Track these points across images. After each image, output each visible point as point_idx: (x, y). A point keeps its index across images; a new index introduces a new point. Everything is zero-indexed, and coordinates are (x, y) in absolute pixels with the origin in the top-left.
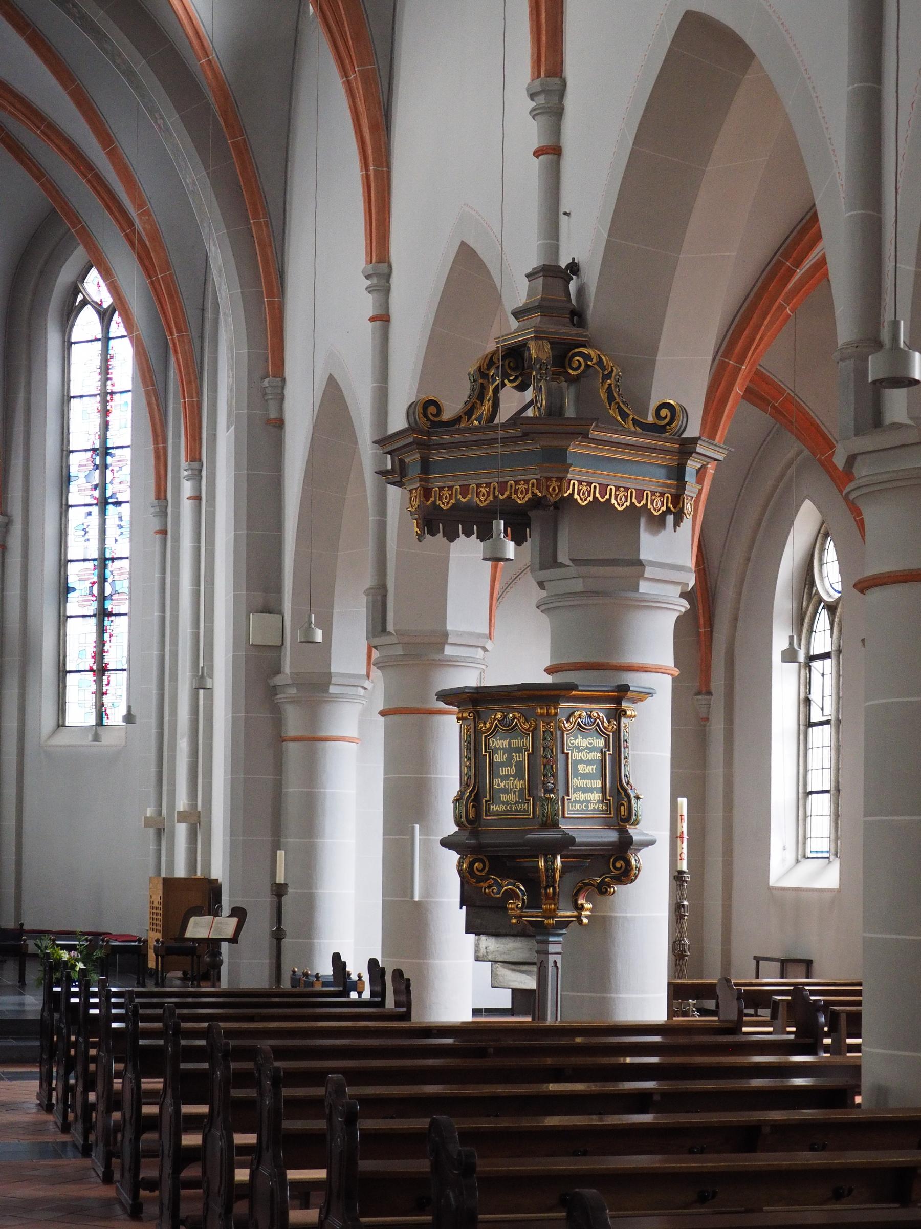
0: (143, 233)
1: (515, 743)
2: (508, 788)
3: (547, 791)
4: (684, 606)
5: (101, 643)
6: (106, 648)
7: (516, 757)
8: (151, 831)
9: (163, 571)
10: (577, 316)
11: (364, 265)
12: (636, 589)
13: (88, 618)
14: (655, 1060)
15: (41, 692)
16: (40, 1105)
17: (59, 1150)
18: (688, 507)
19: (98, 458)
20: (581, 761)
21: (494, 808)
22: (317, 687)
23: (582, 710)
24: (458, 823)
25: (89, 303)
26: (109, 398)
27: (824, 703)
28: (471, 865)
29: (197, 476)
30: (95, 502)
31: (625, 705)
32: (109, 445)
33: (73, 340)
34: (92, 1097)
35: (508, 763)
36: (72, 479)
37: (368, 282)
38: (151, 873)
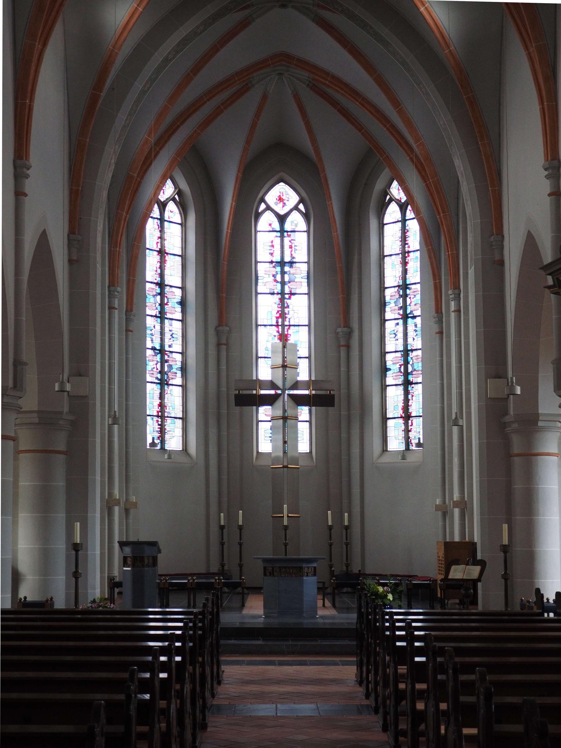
0: (420, 156)
5: (406, 401)
6: (410, 404)
8: (440, 513)
9: (441, 356)
11: (543, 162)
13: (399, 386)
15: (372, 431)
16: (357, 681)
17: (360, 710)
19: (401, 291)
25: (393, 200)
26: (407, 255)
29: (457, 298)
30: (400, 317)
32: (408, 283)
33: (385, 223)
34: (178, 687)
36: (387, 304)
37: (546, 173)
38: (441, 539)
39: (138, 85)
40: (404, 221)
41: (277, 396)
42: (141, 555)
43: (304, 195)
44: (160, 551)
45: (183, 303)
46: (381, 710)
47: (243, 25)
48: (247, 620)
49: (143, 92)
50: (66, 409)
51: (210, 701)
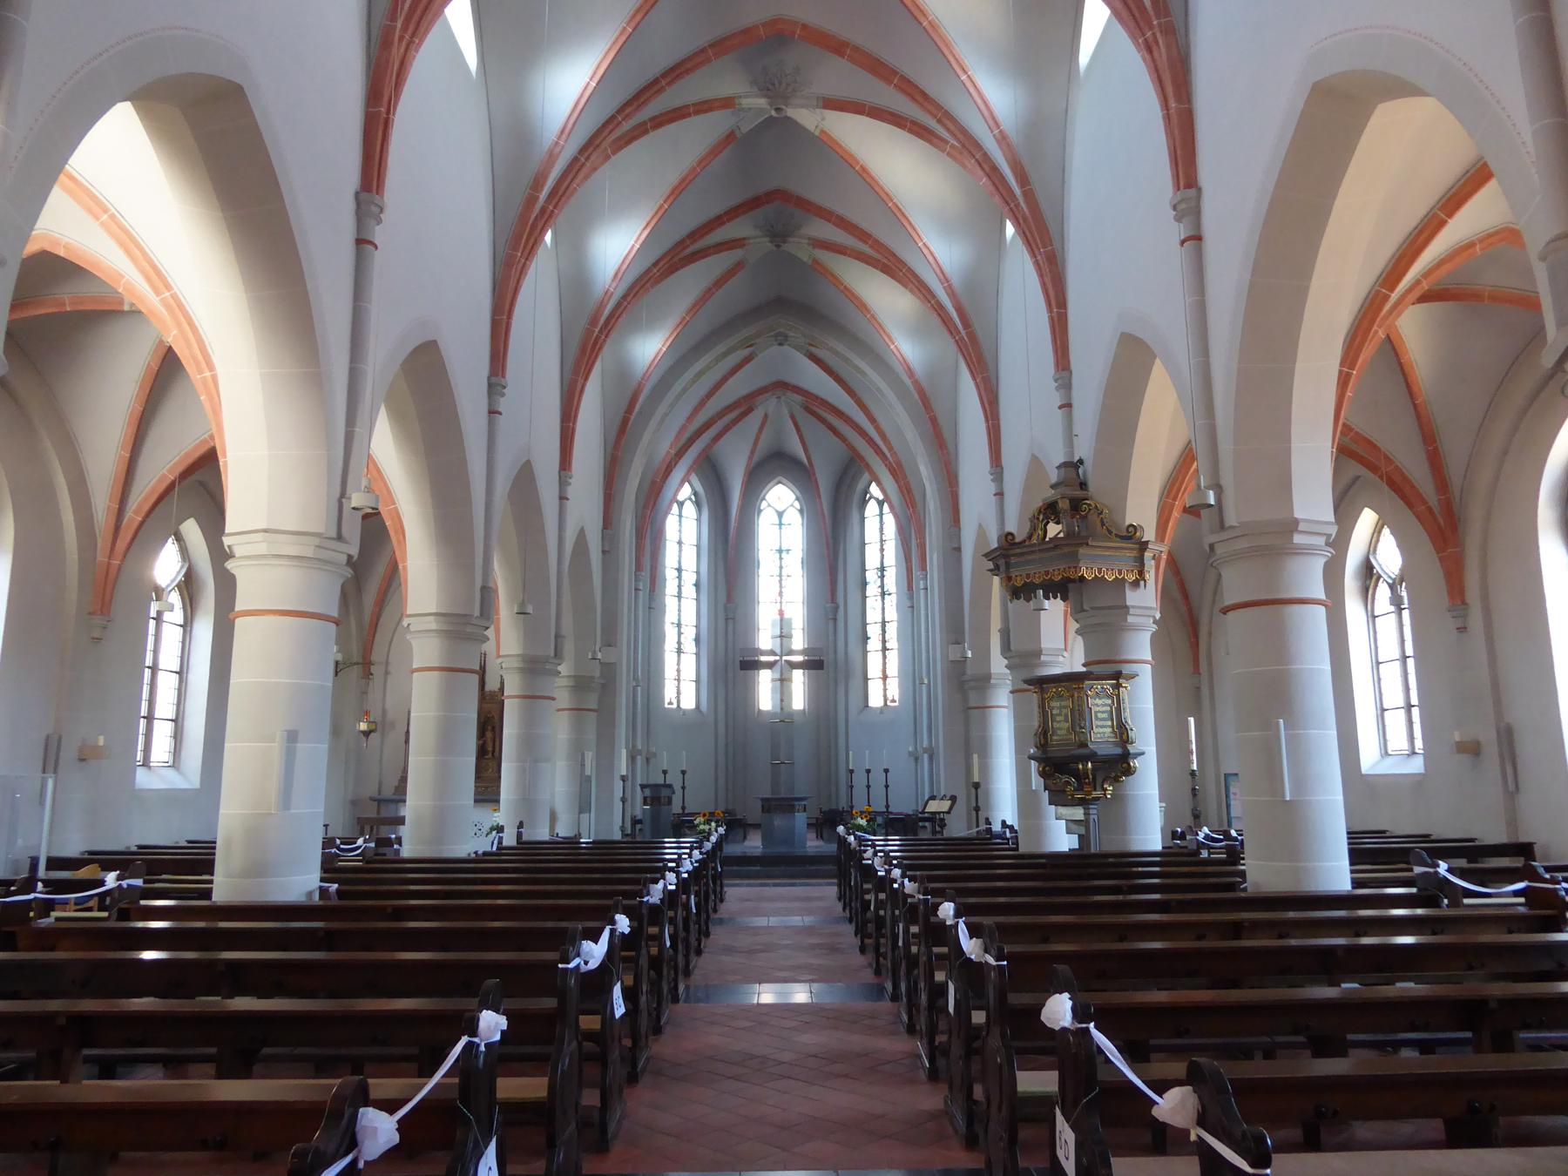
2: (1061, 727)
4: (1154, 628)
10: (1083, 485)
17: (838, 921)
22: (984, 681)
23: (1098, 685)
39: (662, 408)
40: (881, 515)
42: (657, 795)
49: (666, 415)
51: (713, 916)
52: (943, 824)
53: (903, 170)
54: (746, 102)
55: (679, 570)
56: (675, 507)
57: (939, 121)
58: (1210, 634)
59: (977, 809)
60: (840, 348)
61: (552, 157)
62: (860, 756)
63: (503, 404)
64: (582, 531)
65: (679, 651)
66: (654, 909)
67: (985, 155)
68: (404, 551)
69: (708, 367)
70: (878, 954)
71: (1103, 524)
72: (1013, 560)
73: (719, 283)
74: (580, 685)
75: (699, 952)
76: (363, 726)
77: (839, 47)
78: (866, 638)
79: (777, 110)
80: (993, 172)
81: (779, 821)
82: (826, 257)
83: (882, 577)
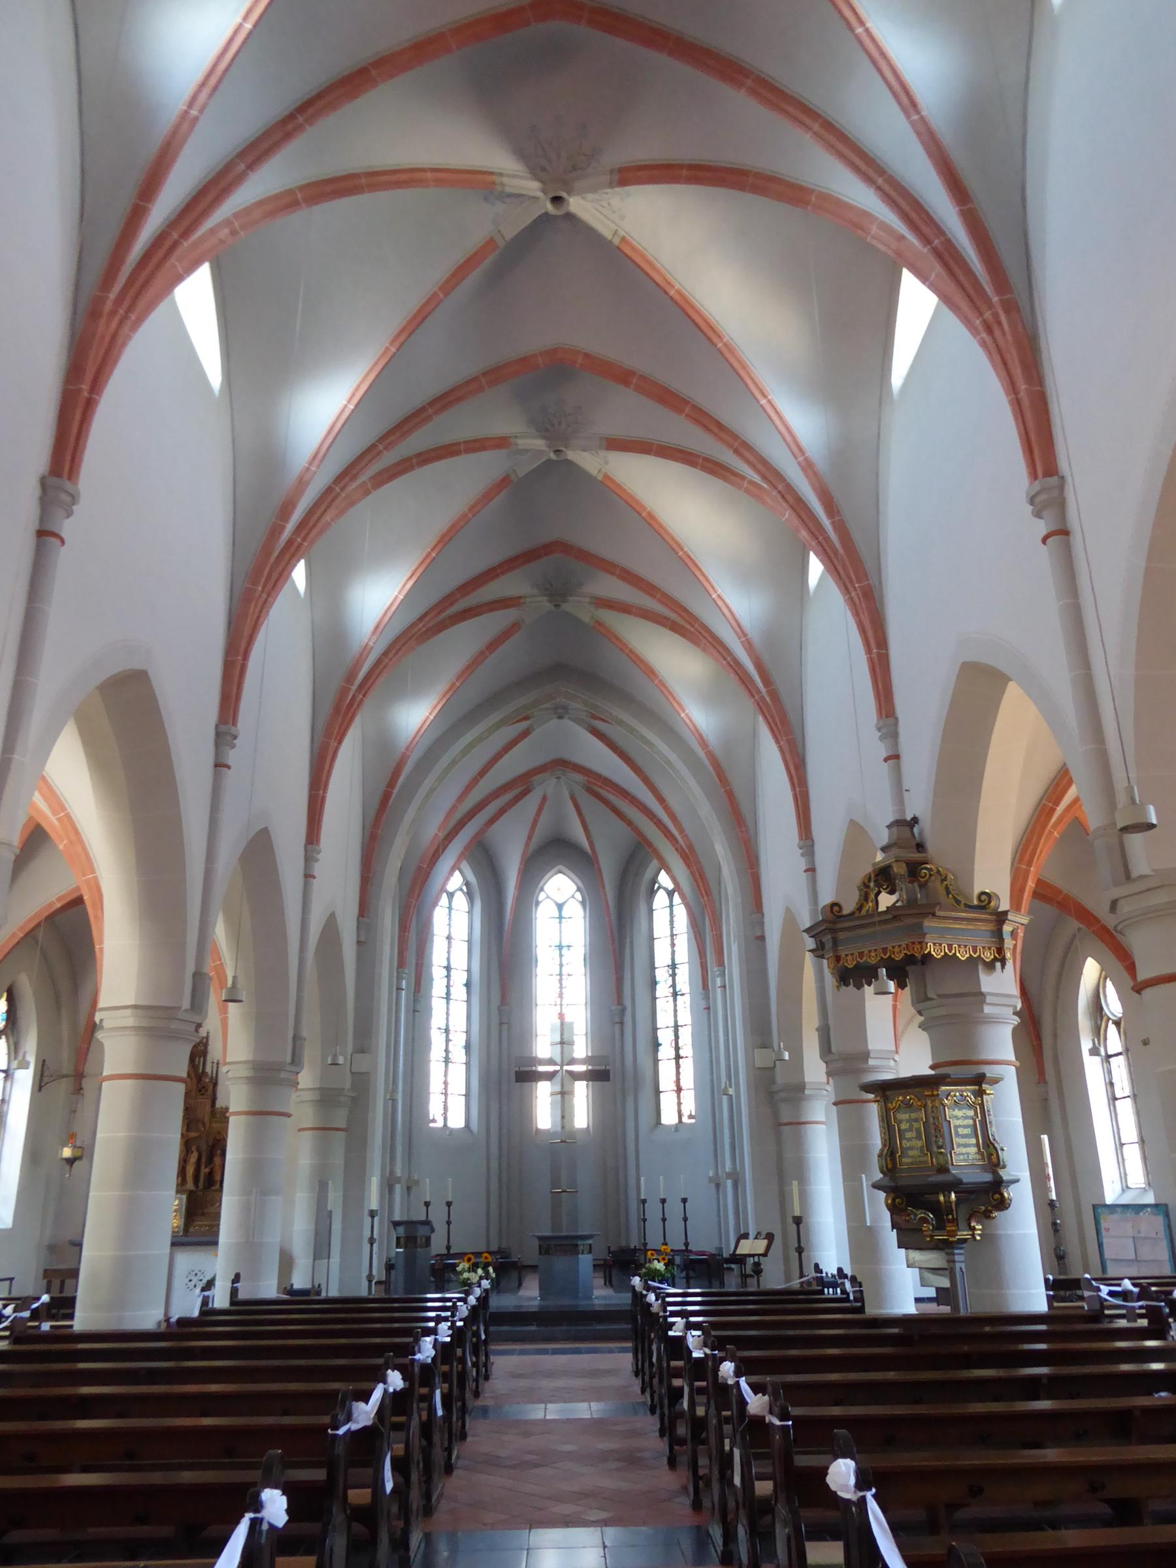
1: (913, 1115)
2: (912, 1145)
3: (940, 1147)
4: (1016, 1020)
7: (915, 1125)
8: (713, 1185)
10: (920, 847)
12: (982, 1010)
14: (1043, 1346)
18: (1008, 955)
20: (960, 1126)
21: (905, 1160)
22: (797, 1091)
24: (882, 1172)
27: (1123, 1086)
28: (894, 1200)
31: (984, 1086)
35: (910, 1129)
39: (428, 783)
40: (671, 906)
41: (554, 1073)
43: (581, 885)
44: (433, 1230)
45: (468, 985)
46: (658, 1411)
47: (525, 734)
48: (525, 1303)
49: (432, 790)
50: (348, 1085)
51: (471, 1403)
52: (758, 1270)
53: (695, 516)
54: (522, 443)
55: (448, 968)
56: (444, 899)
57: (736, 451)
58: (1055, 1035)
59: (800, 1250)
60: (624, 716)
61: (302, 484)
62: (655, 1183)
63: (232, 757)
64: (332, 918)
65: (447, 1060)
66: (424, 1367)
67: (789, 487)
68: (101, 930)
69: (480, 739)
70: (694, 1467)
71: (948, 892)
72: (841, 936)
73: (493, 646)
74: (326, 1098)
75: (449, 1469)
76: (67, 1152)
77: (624, 377)
78: (656, 1045)
79: (557, 452)
80: (798, 505)
81: (560, 1263)
82: (611, 618)
83: (674, 975)
